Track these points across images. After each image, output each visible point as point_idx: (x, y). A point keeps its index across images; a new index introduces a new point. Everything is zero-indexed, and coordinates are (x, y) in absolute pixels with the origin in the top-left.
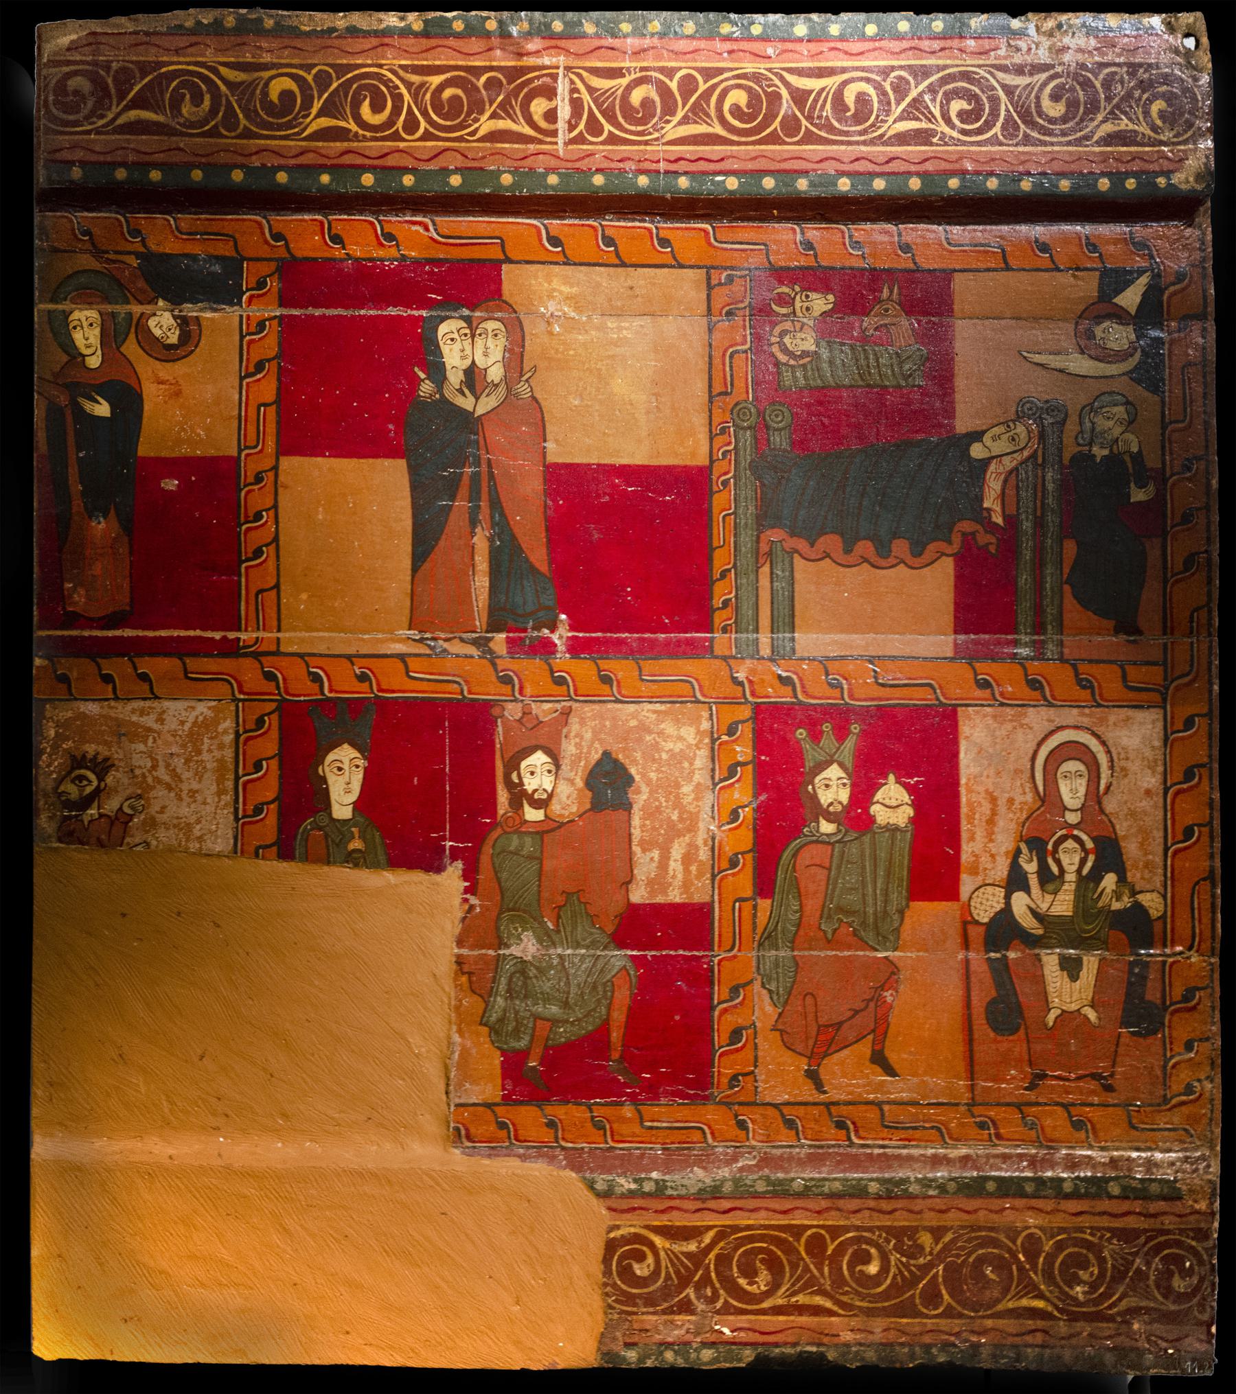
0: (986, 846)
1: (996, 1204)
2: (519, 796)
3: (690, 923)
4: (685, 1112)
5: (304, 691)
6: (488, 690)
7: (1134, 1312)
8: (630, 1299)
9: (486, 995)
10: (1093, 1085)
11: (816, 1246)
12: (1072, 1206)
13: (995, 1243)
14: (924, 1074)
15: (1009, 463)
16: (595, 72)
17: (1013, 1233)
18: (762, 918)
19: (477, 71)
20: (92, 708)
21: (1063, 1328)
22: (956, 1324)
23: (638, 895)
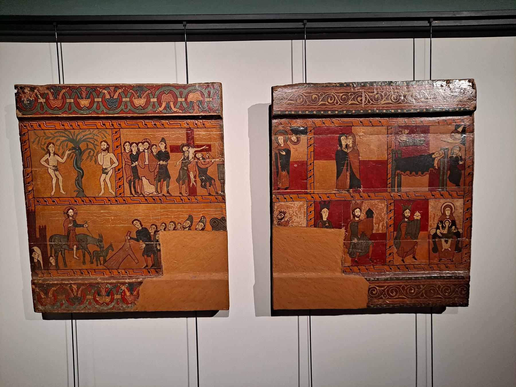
0: (433, 223)
1: (433, 280)
2: (354, 216)
3: (383, 236)
4: (382, 267)
5: (318, 200)
6: (349, 198)
7: (456, 297)
8: (372, 297)
9: (349, 249)
10: (449, 261)
11: (403, 288)
12: (446, 280)
13: (433, 287)
14: (421, 260)
15: (439, 158)
16: (369, 92)
17: (436, 285)
18: (395, 235)
19: (348, 93)
20: (283, 203)
21: (444, 300)
22: (426, 300)
23: (374, 232)
